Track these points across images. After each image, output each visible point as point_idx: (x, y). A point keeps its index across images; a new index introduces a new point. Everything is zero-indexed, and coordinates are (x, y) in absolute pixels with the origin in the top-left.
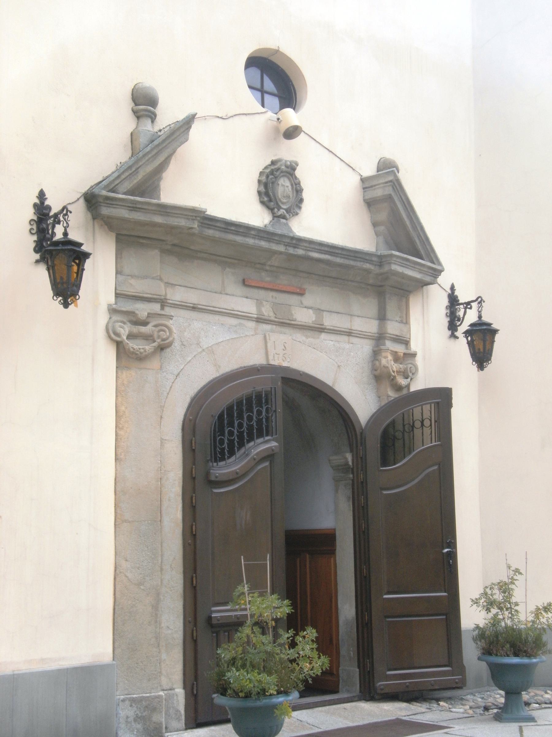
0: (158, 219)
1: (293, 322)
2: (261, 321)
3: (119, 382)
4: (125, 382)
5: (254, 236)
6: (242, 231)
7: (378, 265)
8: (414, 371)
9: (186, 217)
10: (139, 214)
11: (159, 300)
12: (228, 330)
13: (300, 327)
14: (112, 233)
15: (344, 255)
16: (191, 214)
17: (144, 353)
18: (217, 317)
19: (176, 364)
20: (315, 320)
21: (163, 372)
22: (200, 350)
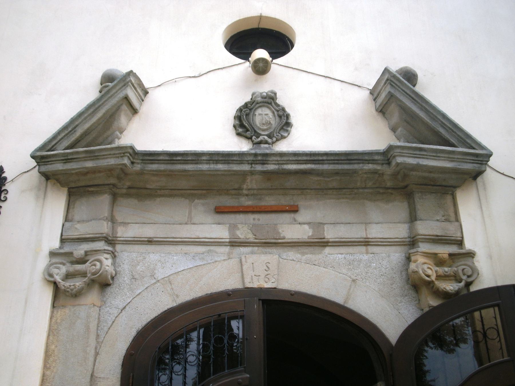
0: (89, 164)
1: (280, 241)
2: (237, 244)
3: (53, 321)
4: (59, 321)
5: (208, 162)
6: (191, 159)
7: (386, 164)
8: (470, 273)
9: (114, 156)
10: (72, 164)
11: (101, 239)
12: (193, 258)
13: (292, 244)
14: (64, 188)
15: (332, 160)
16: (119, 152)
17: (75, 290)
18: (179, 248)
19: (123, 298)
20: (312, 235)
21: (106, 307)
22: (154, 281)
